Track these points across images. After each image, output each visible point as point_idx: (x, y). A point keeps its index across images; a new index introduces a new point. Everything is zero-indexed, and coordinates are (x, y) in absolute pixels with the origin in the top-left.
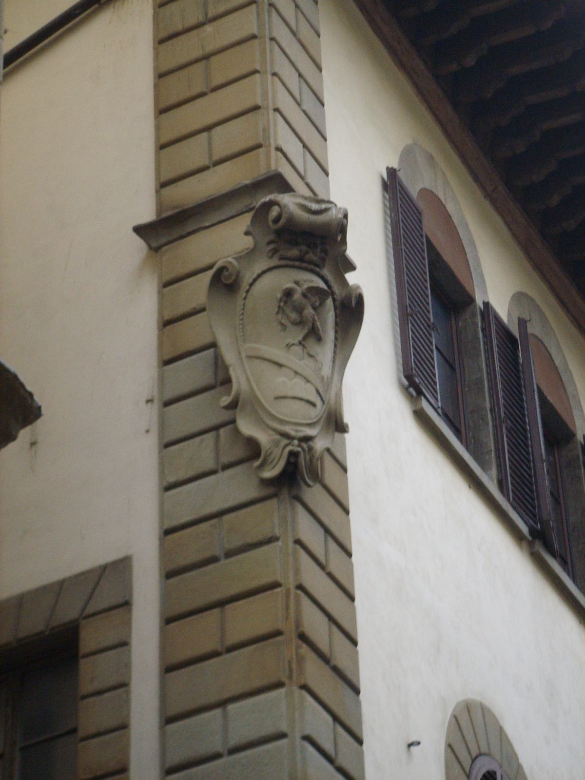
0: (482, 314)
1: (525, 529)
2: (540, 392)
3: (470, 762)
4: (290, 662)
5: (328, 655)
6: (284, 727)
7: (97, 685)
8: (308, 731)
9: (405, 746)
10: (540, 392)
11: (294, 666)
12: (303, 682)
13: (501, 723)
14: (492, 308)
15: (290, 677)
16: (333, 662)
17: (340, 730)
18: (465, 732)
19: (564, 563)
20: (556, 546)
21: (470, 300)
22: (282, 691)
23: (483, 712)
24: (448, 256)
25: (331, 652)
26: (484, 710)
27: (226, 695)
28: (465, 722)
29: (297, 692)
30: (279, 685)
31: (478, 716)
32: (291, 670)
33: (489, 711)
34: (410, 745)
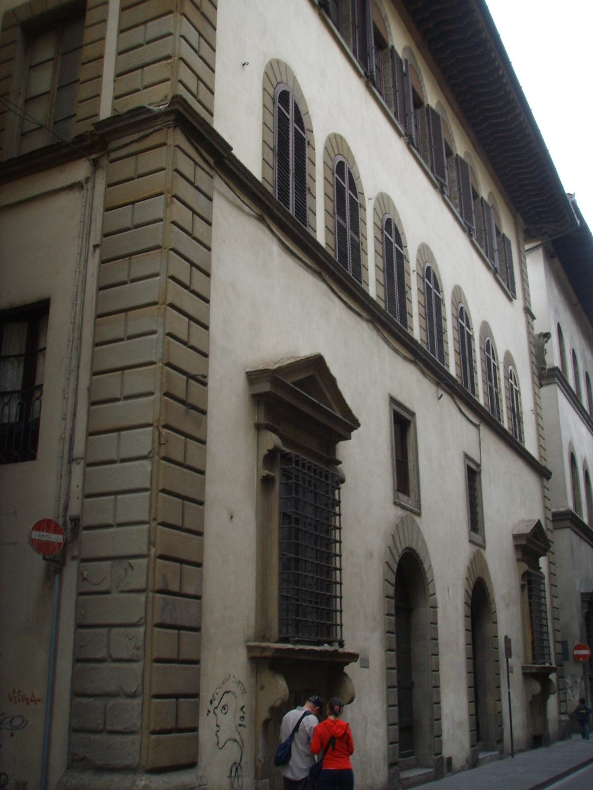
0: (426, 110)
1: (362, 73)
2: (375, 26)
3: (276, 84)
4: (177, 3)
5: (199, 6)
6: (171, 30)
7: (94, 21)
8: (183, 33)
9: (240, 65)
10: (375, 26)
11: (179, 4)
12: (182, 12)
13: (295, 75)
14: (396, 51)
15: (176, 9)
16: (202, 10)
17: (202, 40)
18: (332, 143)
19: (418, 150)
20: (415, 145)
21: (386, 45)
22: (171, 16)
23: (286, 69)
24: (382, 31)
25: (201, 5)
26: (388, 198)
27: (146, 18)
28: (333, 141)
29: (179, 17)
30: (171, 12)
31: (339, 140)
32: (177, 6)
33: (289, 67)
34: (244, 65)
